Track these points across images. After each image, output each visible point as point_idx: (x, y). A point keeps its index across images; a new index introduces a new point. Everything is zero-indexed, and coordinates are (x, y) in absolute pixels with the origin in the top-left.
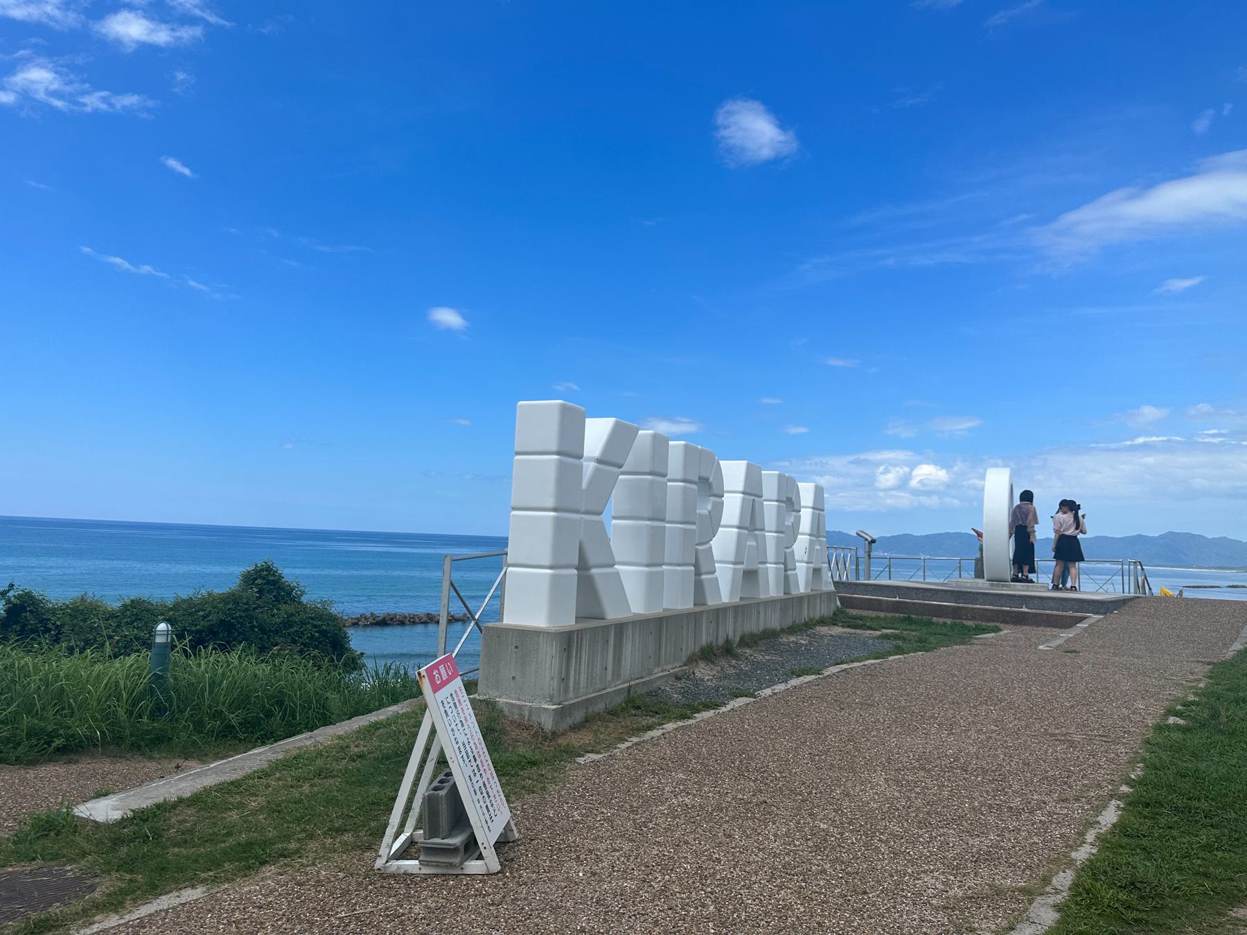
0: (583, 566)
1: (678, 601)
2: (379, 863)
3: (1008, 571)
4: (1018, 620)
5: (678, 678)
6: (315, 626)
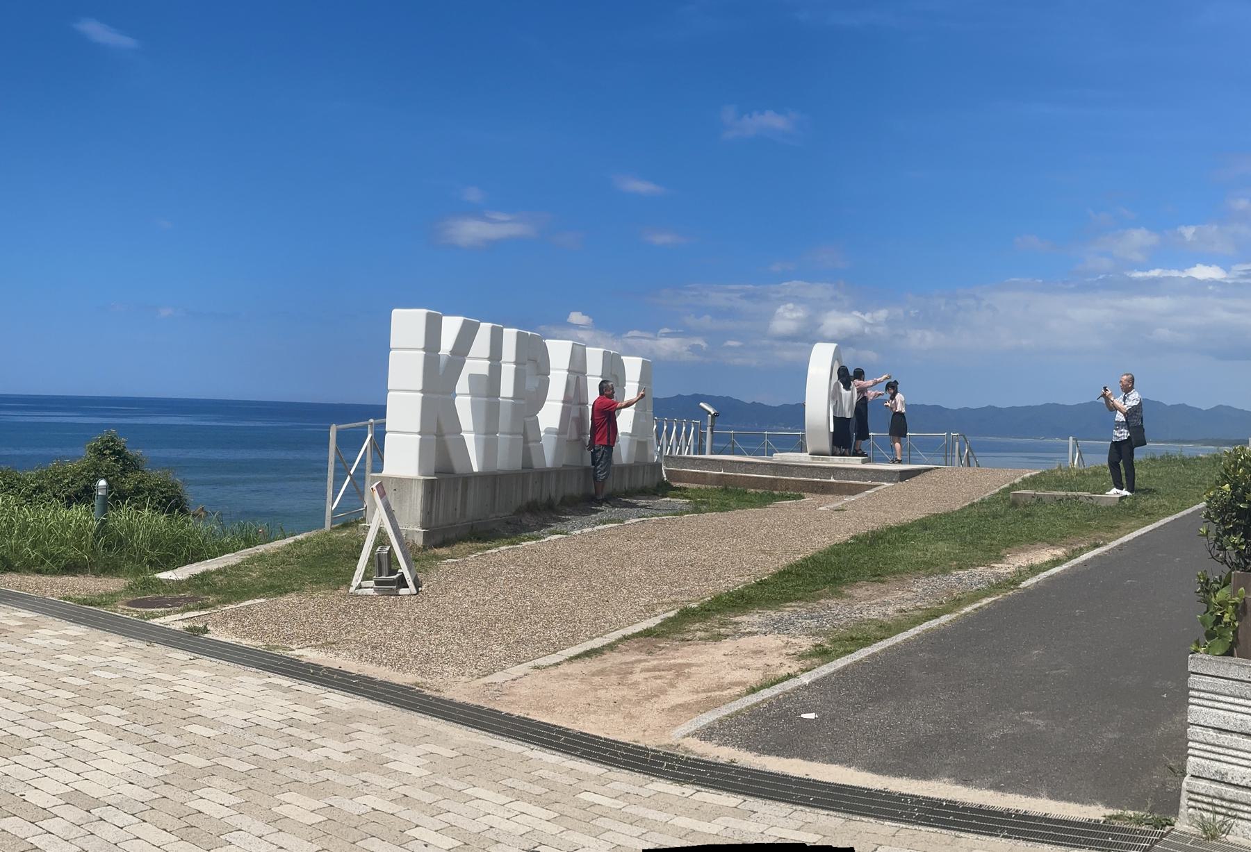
0: (440, 434)
1: (505, 461)
2: (352, 590)
3: (826, 445)
4: (825, 489)
5: (508, 523)
6: (162, 493)
